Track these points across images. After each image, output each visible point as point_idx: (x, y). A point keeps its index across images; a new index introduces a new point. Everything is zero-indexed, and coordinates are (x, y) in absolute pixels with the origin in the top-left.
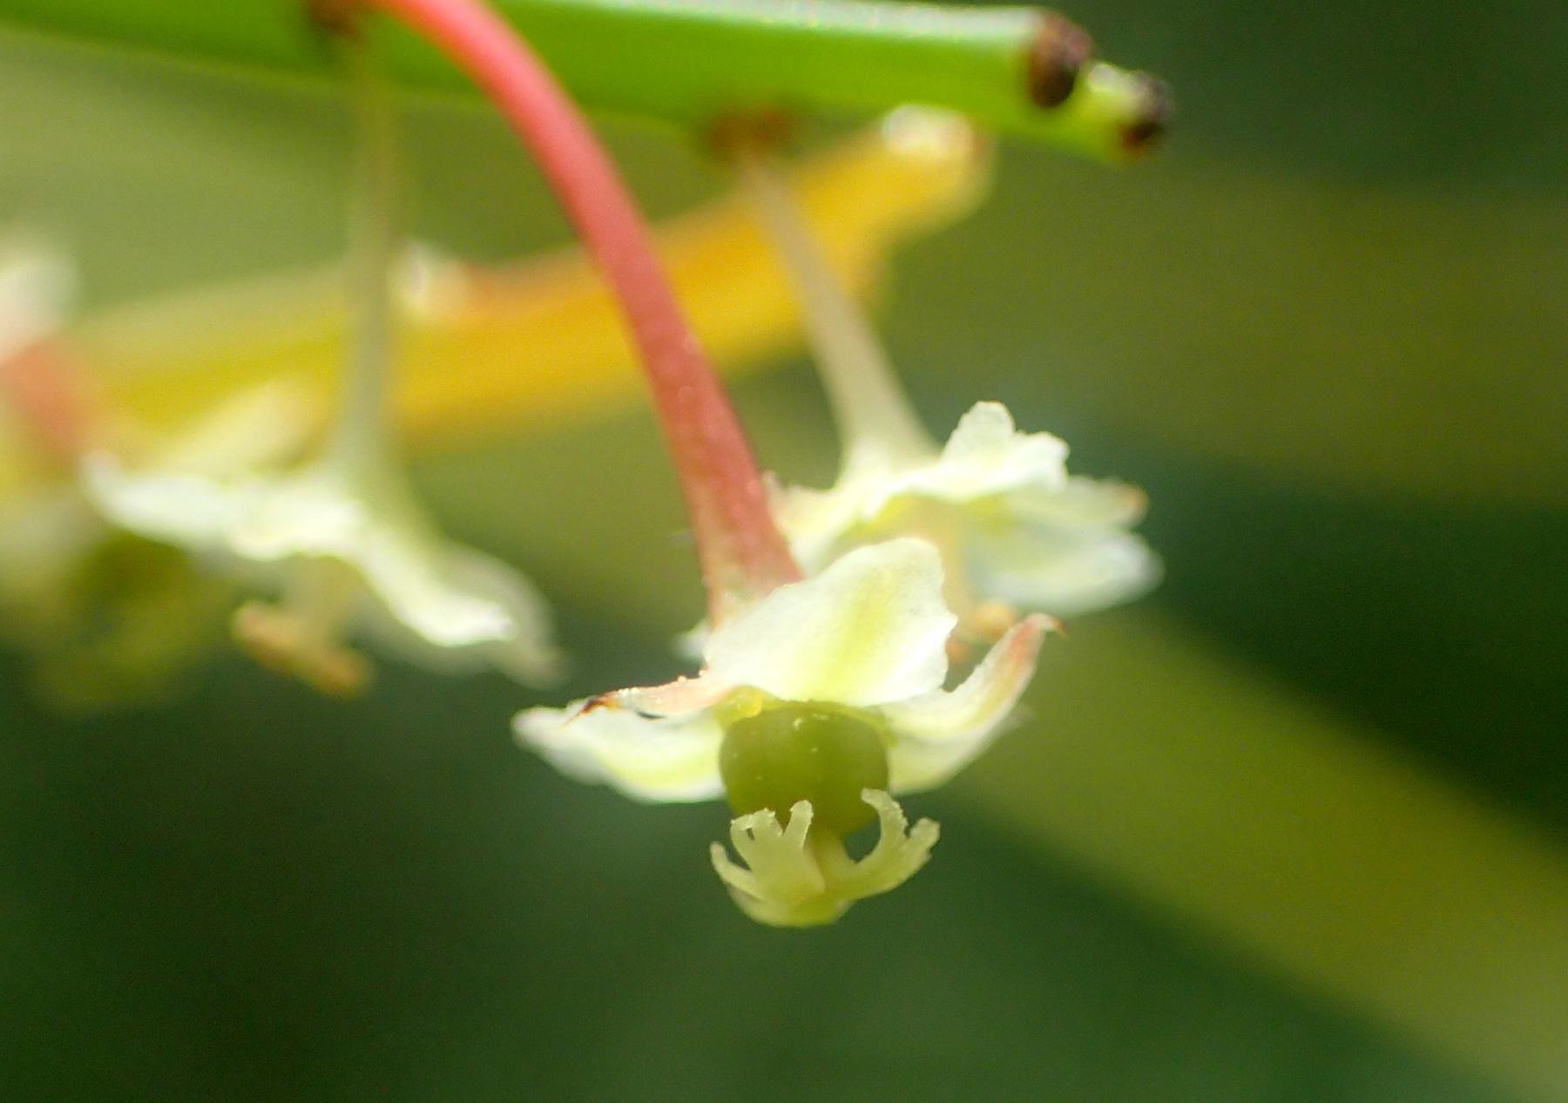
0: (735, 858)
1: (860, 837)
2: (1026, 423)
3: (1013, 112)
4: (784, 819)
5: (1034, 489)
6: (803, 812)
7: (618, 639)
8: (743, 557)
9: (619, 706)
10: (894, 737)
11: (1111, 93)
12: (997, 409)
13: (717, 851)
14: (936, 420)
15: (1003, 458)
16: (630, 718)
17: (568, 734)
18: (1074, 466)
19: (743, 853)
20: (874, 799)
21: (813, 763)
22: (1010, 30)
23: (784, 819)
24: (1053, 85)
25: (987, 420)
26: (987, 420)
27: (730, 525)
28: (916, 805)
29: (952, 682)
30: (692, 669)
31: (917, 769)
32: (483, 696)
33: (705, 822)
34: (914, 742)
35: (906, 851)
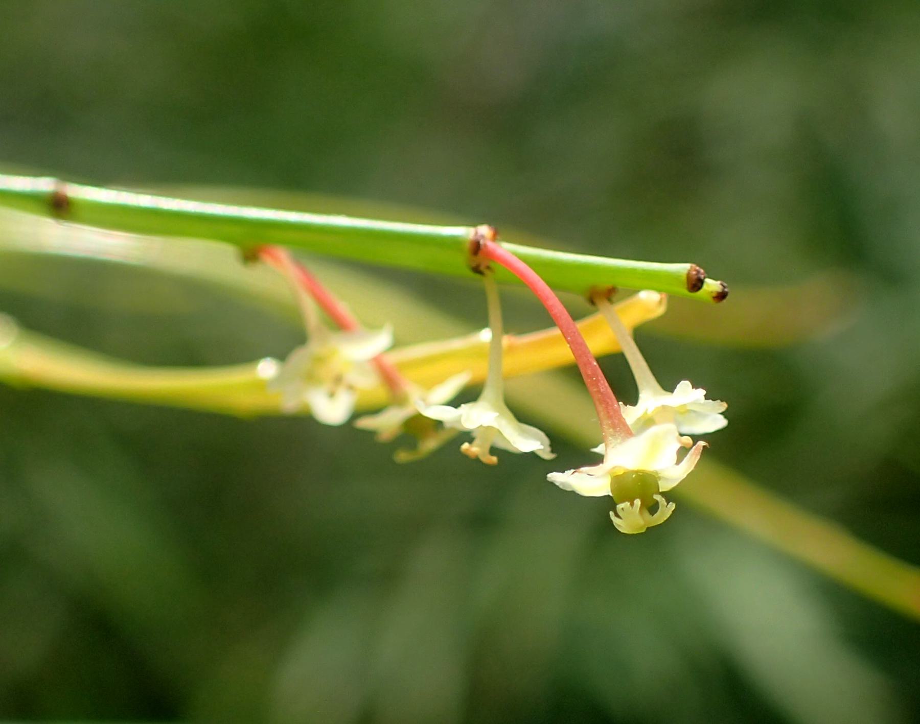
0: (617, 515)
1: (653, 508)
2: (695, 386)
3: (684, 291)
4: (632, 504)
5: (695, 403)
6: (638, 502)
7: (574, 451)
8: (614, 426)
9: (582, 472)
10: (660, 478)
11: (712, 285)
12: (688, 383)
13: (611, 513)
14: (669, 386)
15: (688, 394)
16: (585, 475)
17: (555, 477)
18: (707, 397)
19: (620, 514)
20: (658, 497)
21: (640, 487)
22: (682, 268)
23: (632, 504)
24: (696, 284)
25: (684, 386)
26: (684, 386)
27: (610, 417)
28: (669, 496)
29: (678, 462)
30: (597, 460)
31: (665, 487)
32: (514, 465)
33: (607, 504)
34: (666, 479)
35: (667, 510)
